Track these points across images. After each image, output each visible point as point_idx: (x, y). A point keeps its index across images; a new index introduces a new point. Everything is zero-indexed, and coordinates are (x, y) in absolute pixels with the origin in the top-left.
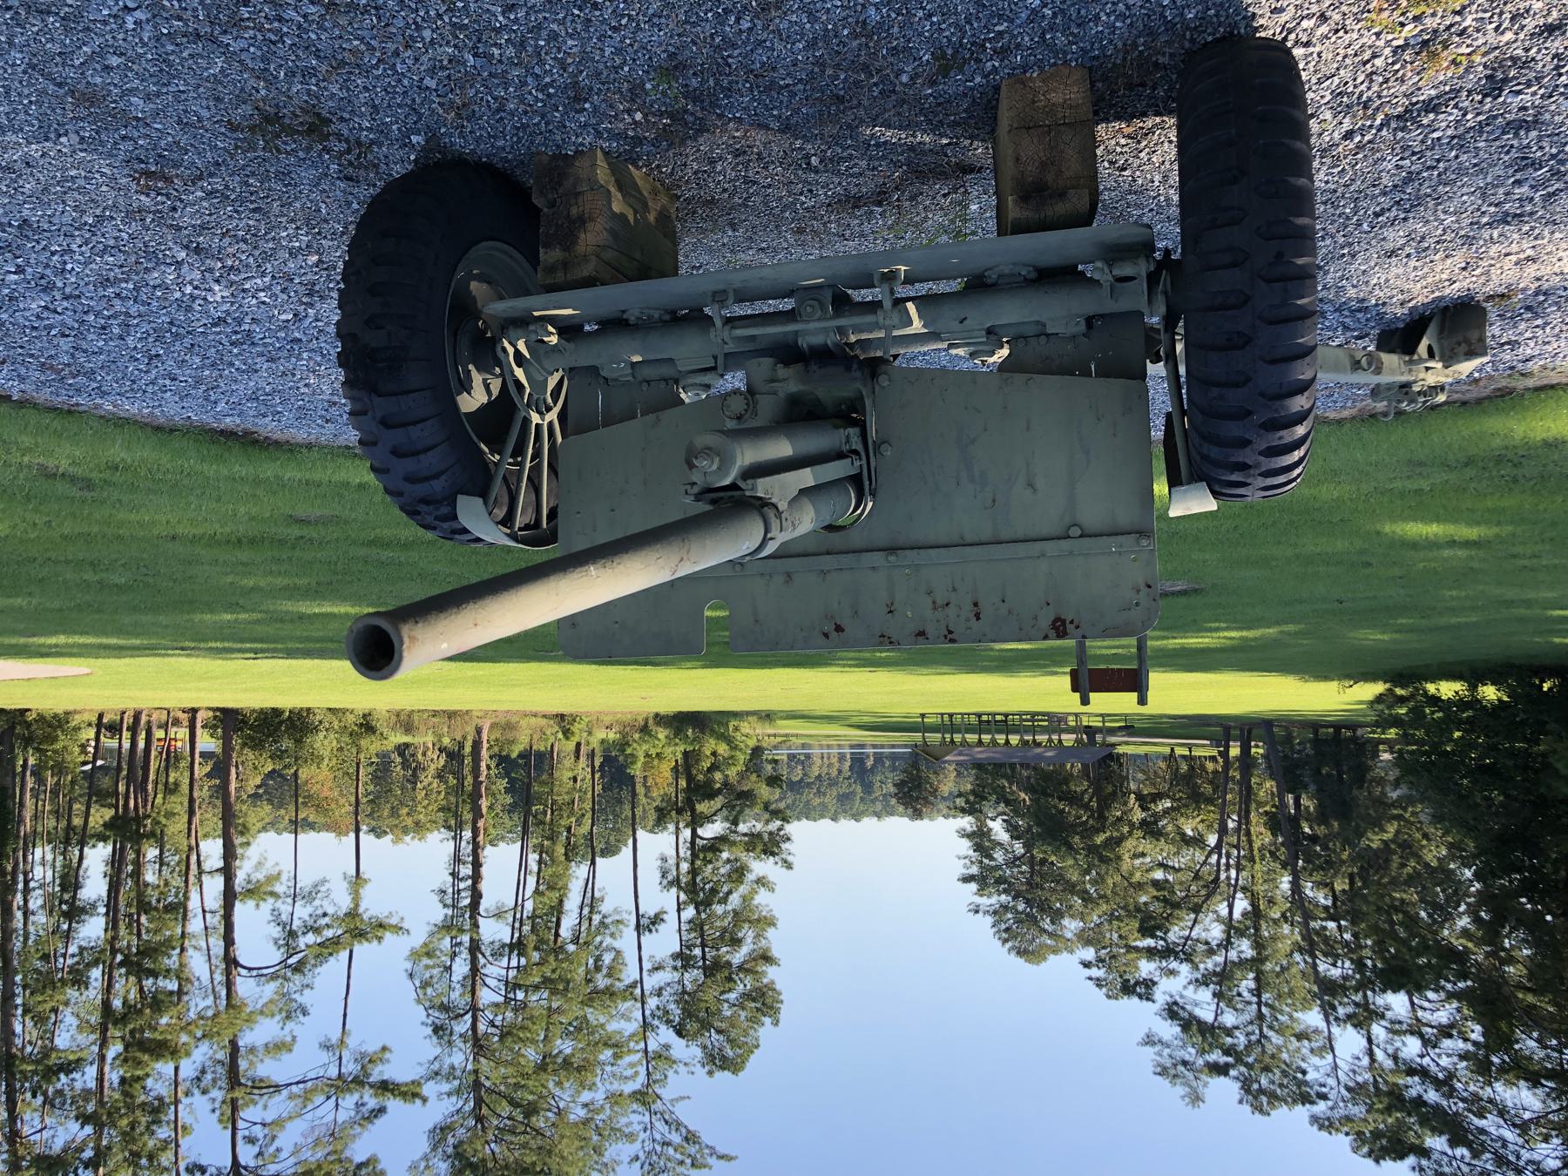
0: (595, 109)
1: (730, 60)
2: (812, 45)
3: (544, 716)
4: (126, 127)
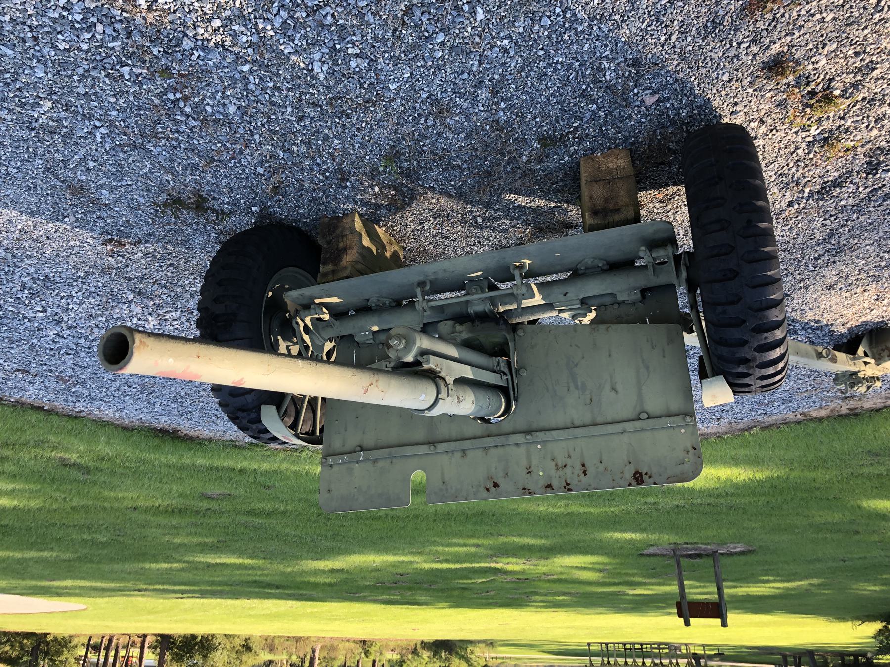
0: (353, 187)
1: (425, 148)
2: (469, 136)
3: (354, 642)
4: (100, 210)
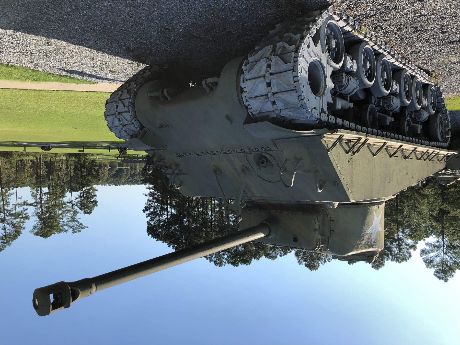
3: (52, 154)
